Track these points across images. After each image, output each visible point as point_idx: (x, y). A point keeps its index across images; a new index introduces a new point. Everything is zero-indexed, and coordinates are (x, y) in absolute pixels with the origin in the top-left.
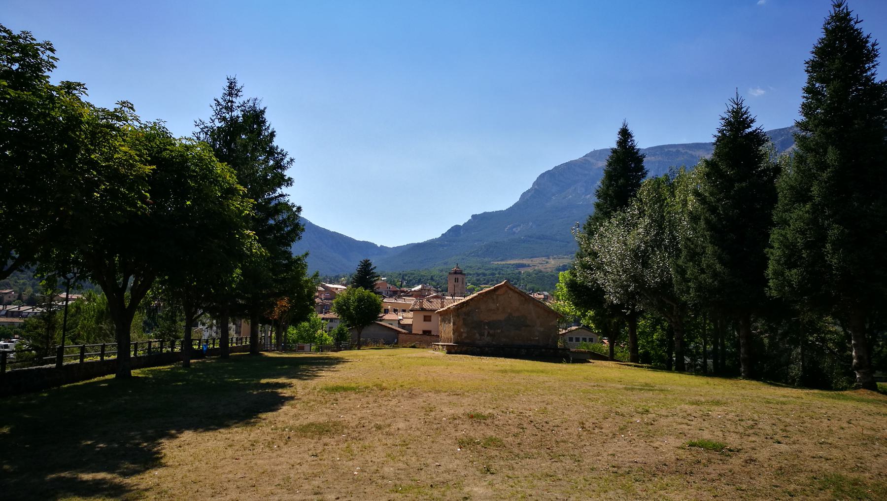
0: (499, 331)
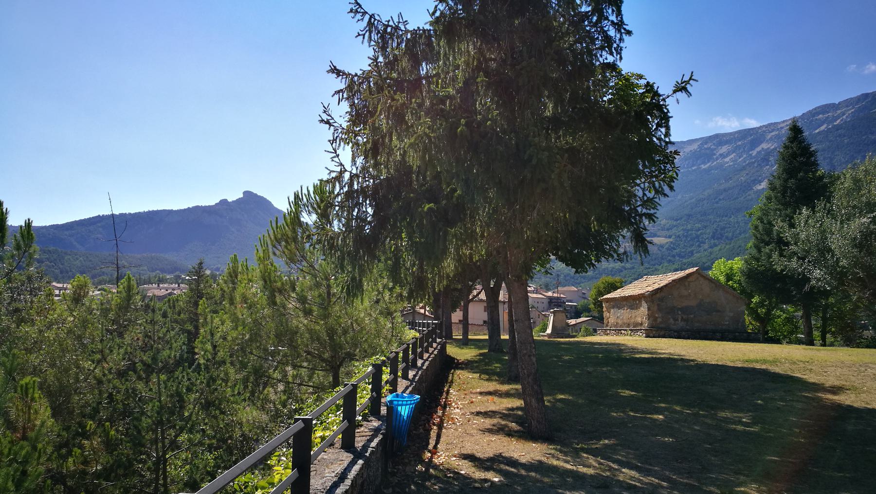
0: (692, 316)
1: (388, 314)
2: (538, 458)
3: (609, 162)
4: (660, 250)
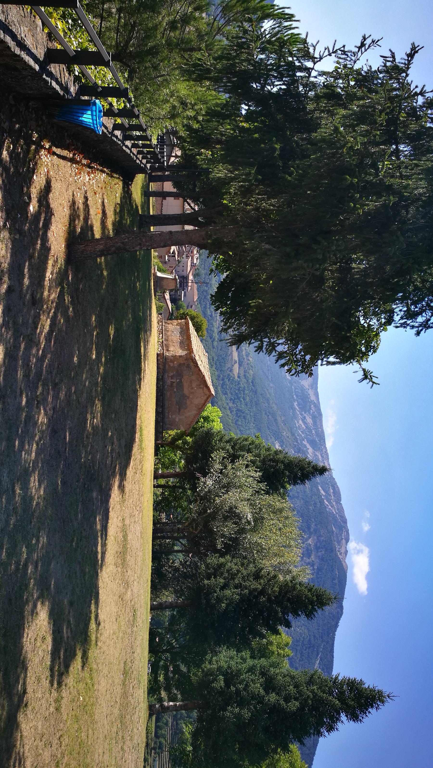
0: (175, 390)
1: (173, 116)
2: (52, 247)
3: (309, 312)
4: (228, 369)
